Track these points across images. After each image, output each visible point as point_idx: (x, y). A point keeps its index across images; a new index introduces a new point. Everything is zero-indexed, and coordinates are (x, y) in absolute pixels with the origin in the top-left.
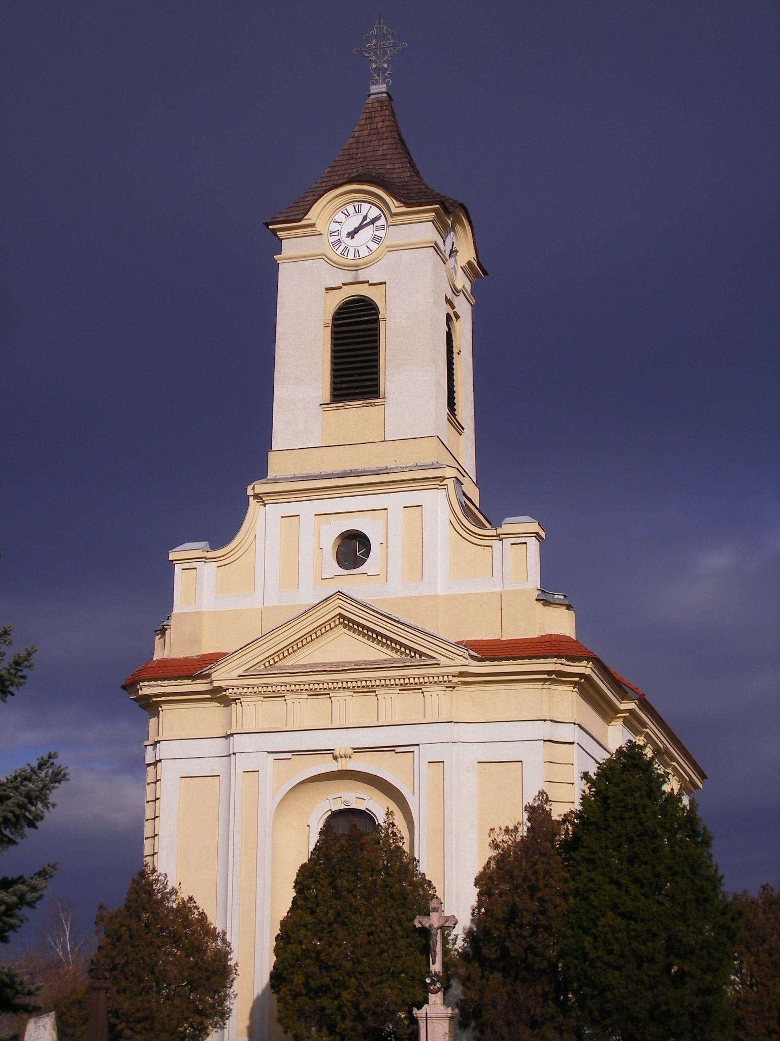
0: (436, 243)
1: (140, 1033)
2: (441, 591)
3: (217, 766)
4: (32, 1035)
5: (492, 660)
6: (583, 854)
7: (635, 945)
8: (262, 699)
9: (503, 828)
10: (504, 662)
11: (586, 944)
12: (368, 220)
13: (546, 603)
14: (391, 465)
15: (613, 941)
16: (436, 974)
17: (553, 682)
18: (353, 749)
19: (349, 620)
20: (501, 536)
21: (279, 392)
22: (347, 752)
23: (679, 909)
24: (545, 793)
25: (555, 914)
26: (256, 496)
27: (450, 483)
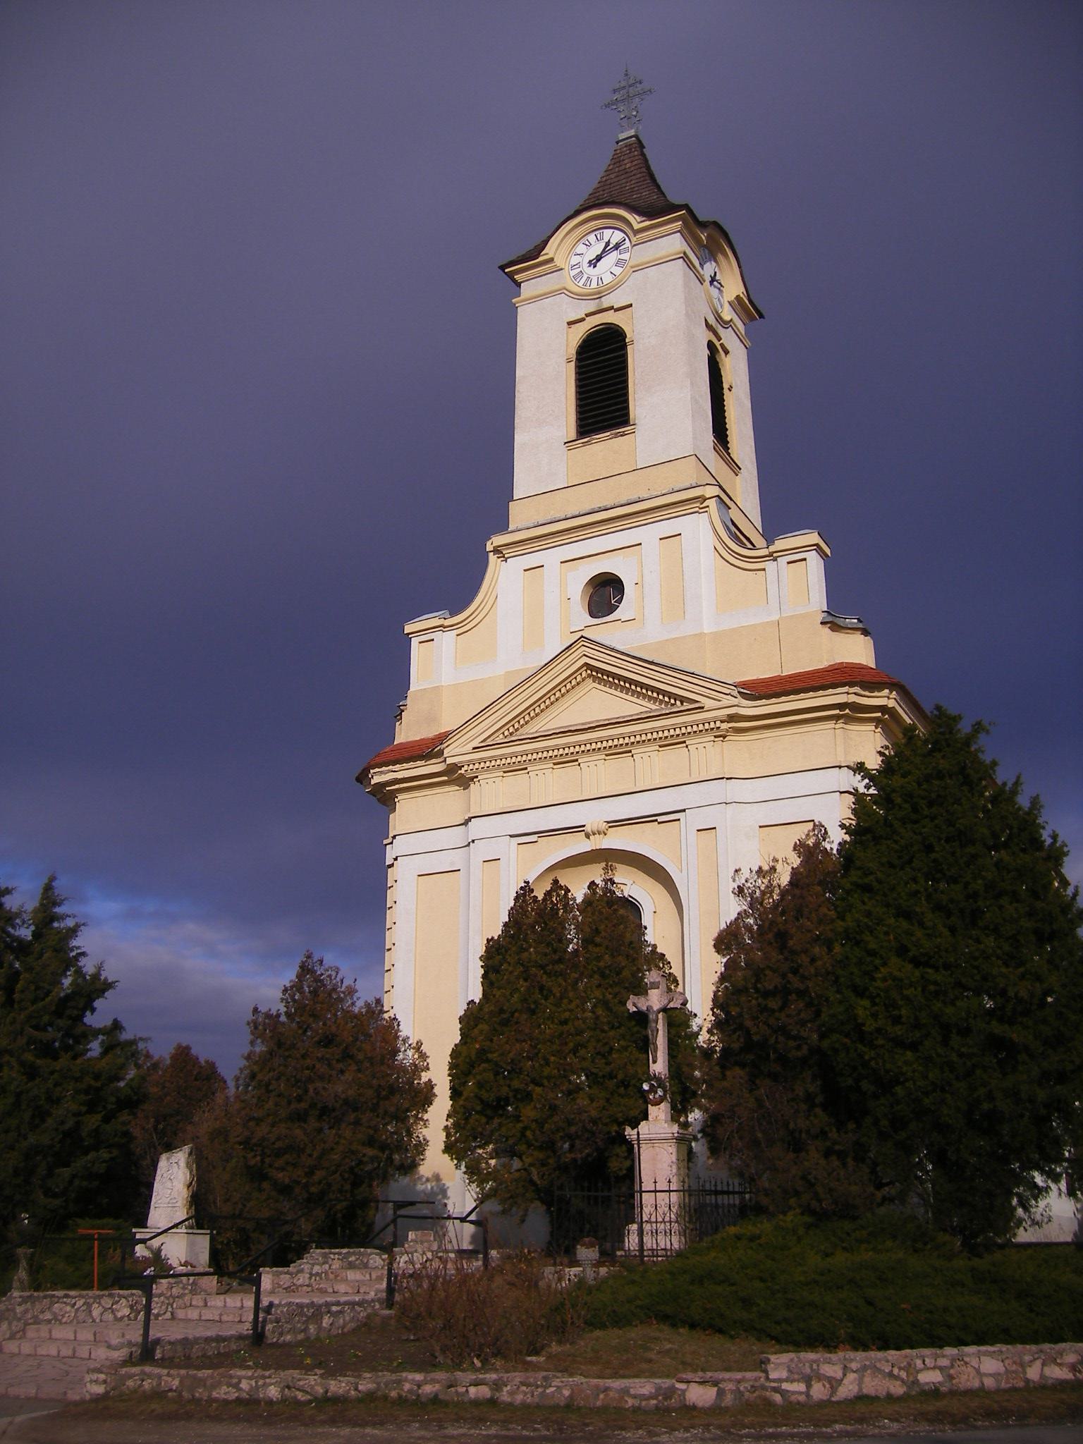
0: (685, 253)
1: (283, 1169)
4: (165, 1175)
5: (768, 697)
6: (855, 879)
7: (937, 1006)
8: (502, 774)
9: (755, 868)
10: (783, 699)
11: (860, 1012)
12: (611, 246)
13: (835, 627)
15: (900, 1003)
16: (658, 1079)
17: (849, 720)
18: (608, 822)
19: (598, 670)
20: (775, 555)
21: (520, 438)
22: (600, 826)
23: (1007, 948)
24: (823, 826)
25: (813, 971)
26: (497, 551)
27: (712, 504)
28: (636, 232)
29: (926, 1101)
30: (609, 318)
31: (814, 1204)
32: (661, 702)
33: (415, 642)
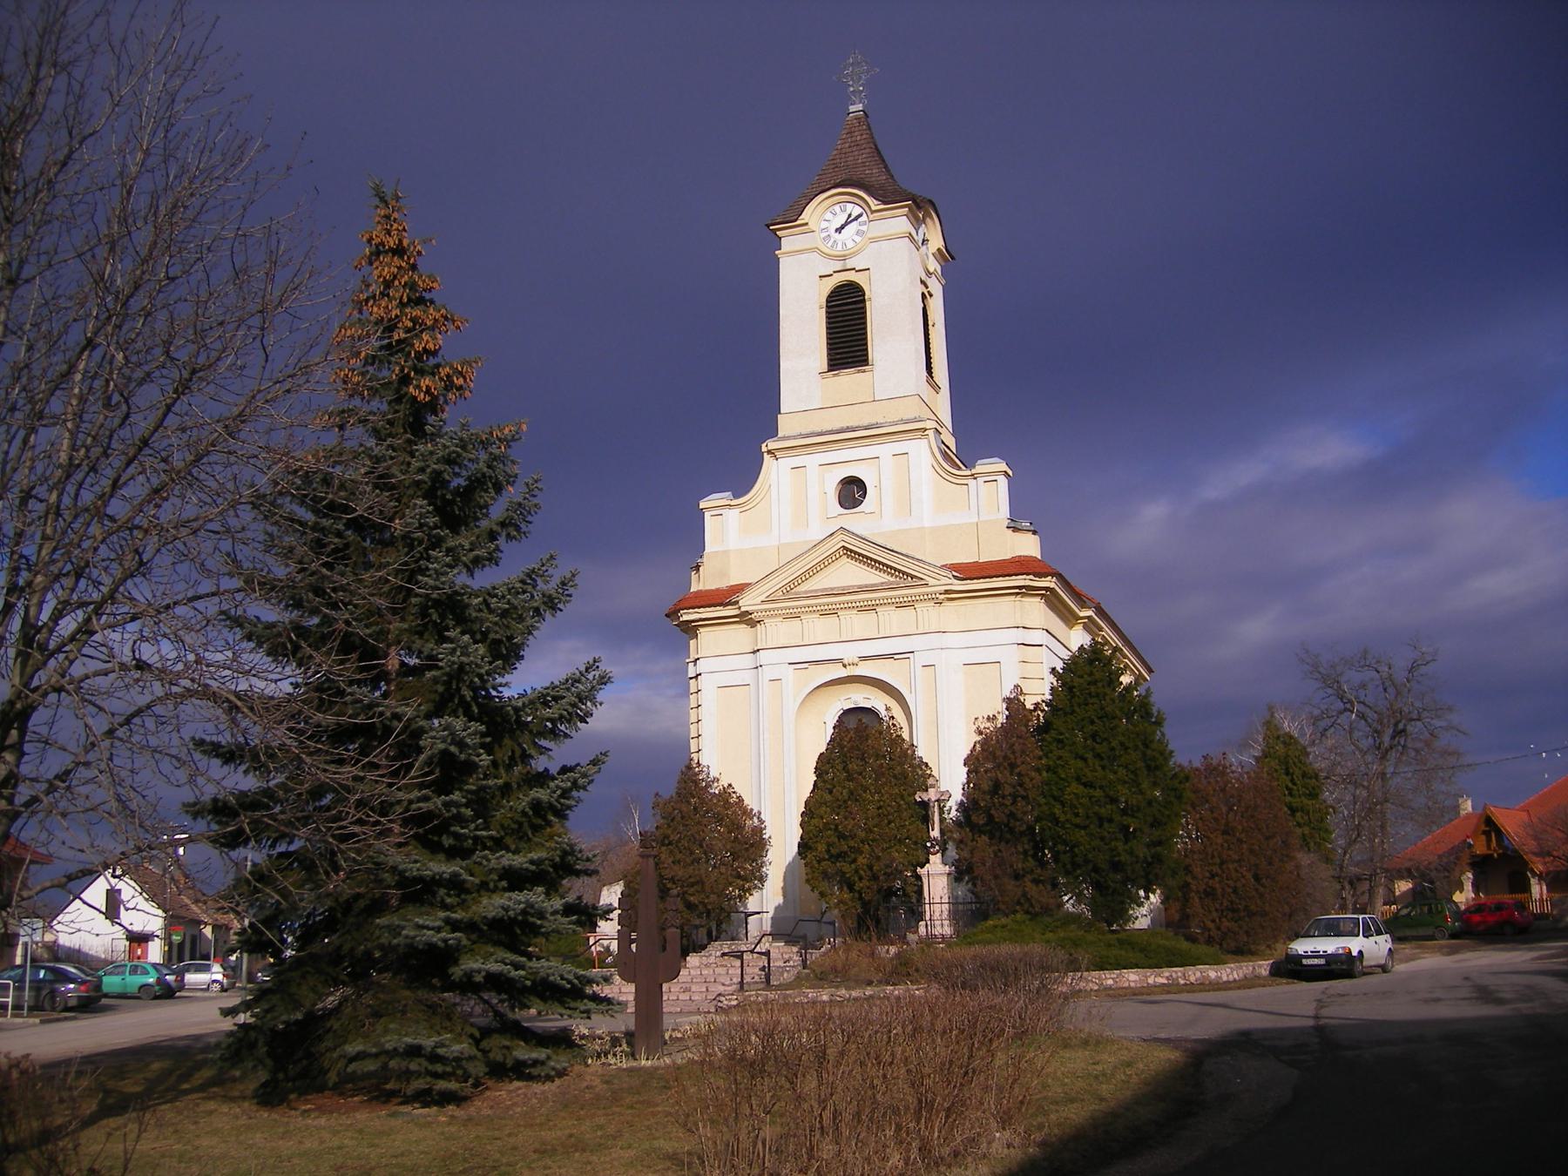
2: (927, 523)
3: (747, 677)
12: (852, 217)
13: (1016, 530)
14: (881, 420)
16: (935, 839)
17: (1023, 595)
19: (851, 551)
21: (785, 365)
26: (769, 452)
27: (931, 433)
28: (873, 212)
29: (1090, 856)
30: (851, 276)
31: (1031, 909)
32: (896, 577)
33: (707, 515)
